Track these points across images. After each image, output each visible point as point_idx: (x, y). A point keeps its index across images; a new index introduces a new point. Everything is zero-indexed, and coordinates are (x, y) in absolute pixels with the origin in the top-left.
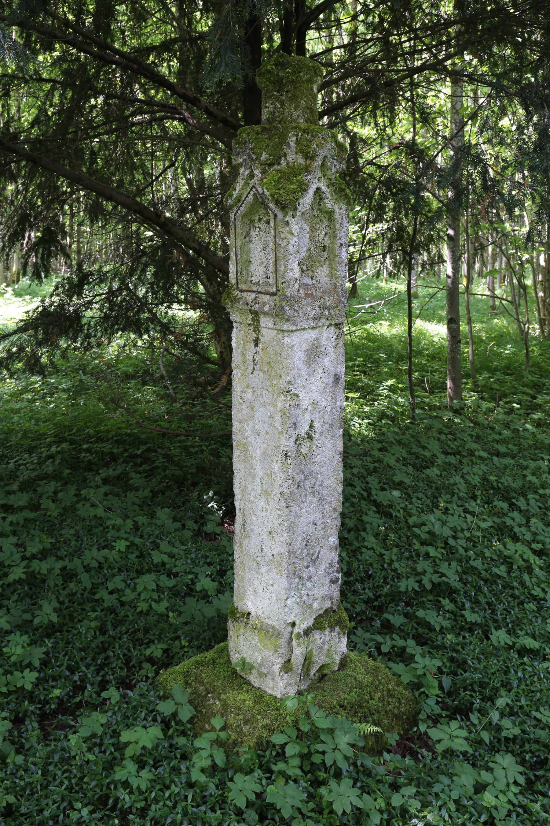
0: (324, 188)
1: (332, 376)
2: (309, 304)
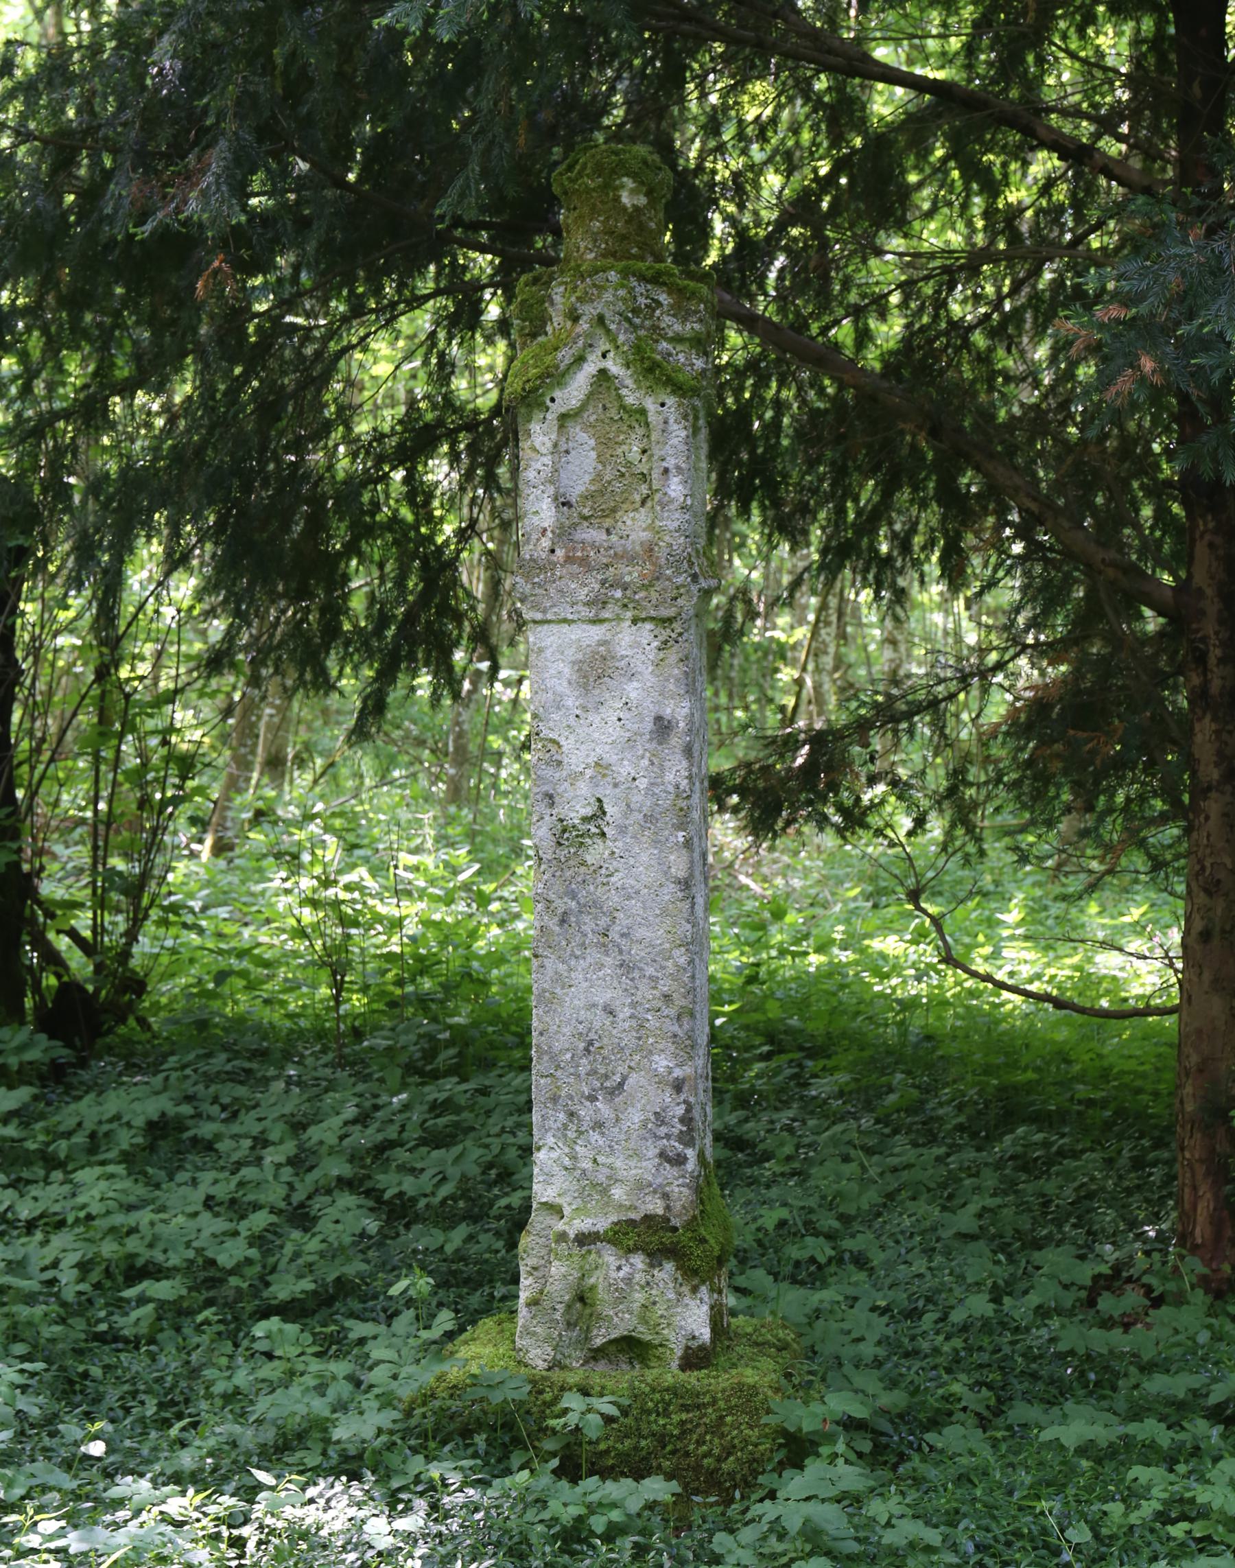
0: (614, 367)
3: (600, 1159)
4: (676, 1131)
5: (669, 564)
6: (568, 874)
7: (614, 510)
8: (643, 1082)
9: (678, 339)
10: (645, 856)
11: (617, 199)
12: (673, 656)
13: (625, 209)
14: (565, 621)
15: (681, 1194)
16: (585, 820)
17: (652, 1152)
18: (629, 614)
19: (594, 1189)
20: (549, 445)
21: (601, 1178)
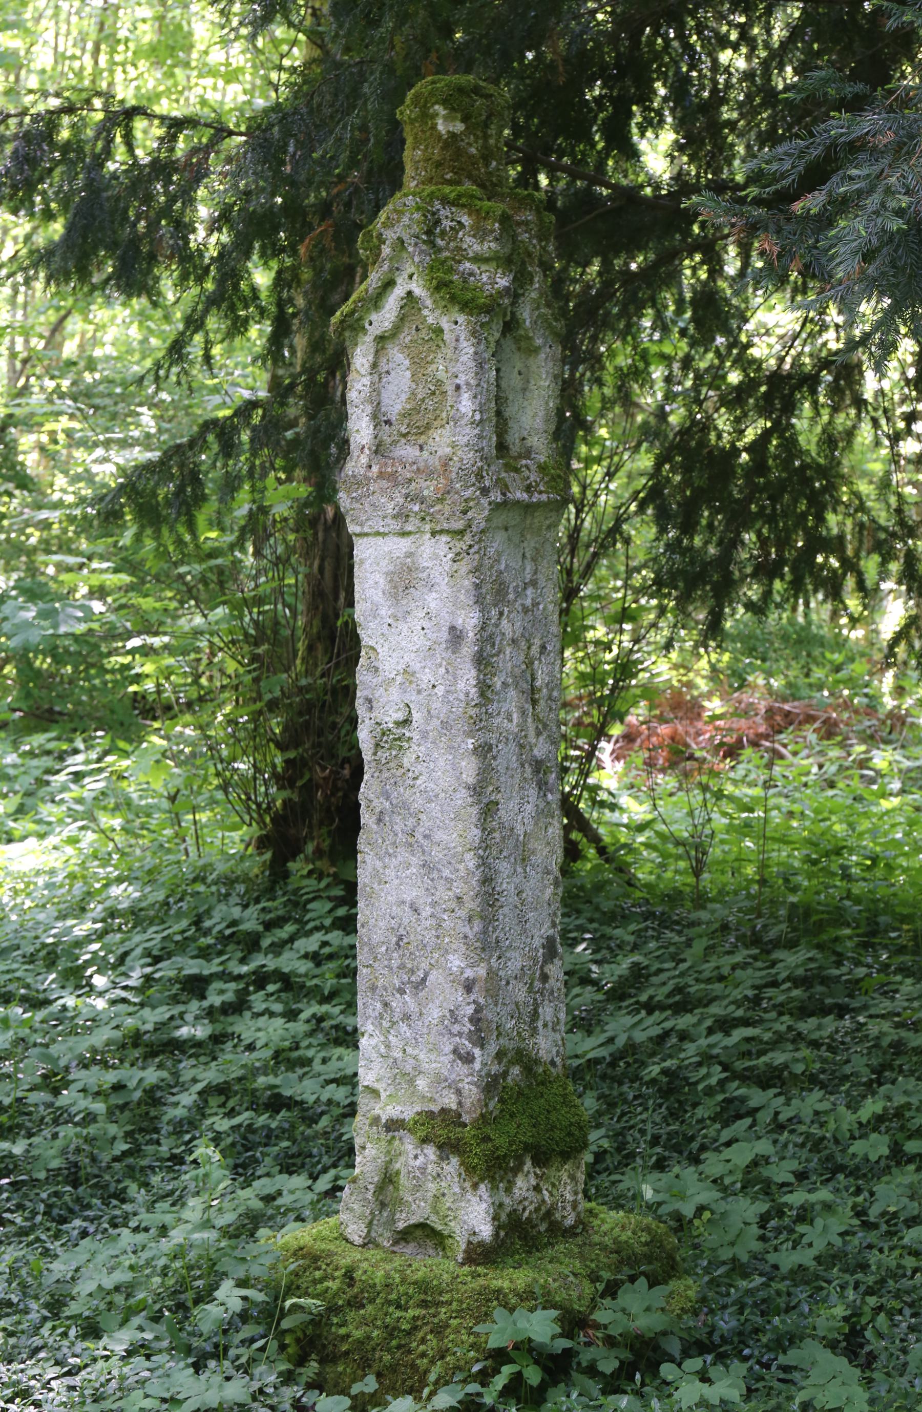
0: (418, 291)
1: (445, 629)
3: (409, 1050)
4: (466, 1030)
5: (460, 479)
6: (386, 774)
7: (428, 427)
8: (441, 979)
9: (478, 259)
10: (442, 761)
11: (434, 127)
12: (464, 567)
13: (440, 136)
14: (378, 534)
15: (472, 1092)
16: (398, 724)
17: (448, 1048)
18: (428, 527)
19: (404, 1078)
20: (367, 366)
21: (408, 1068)
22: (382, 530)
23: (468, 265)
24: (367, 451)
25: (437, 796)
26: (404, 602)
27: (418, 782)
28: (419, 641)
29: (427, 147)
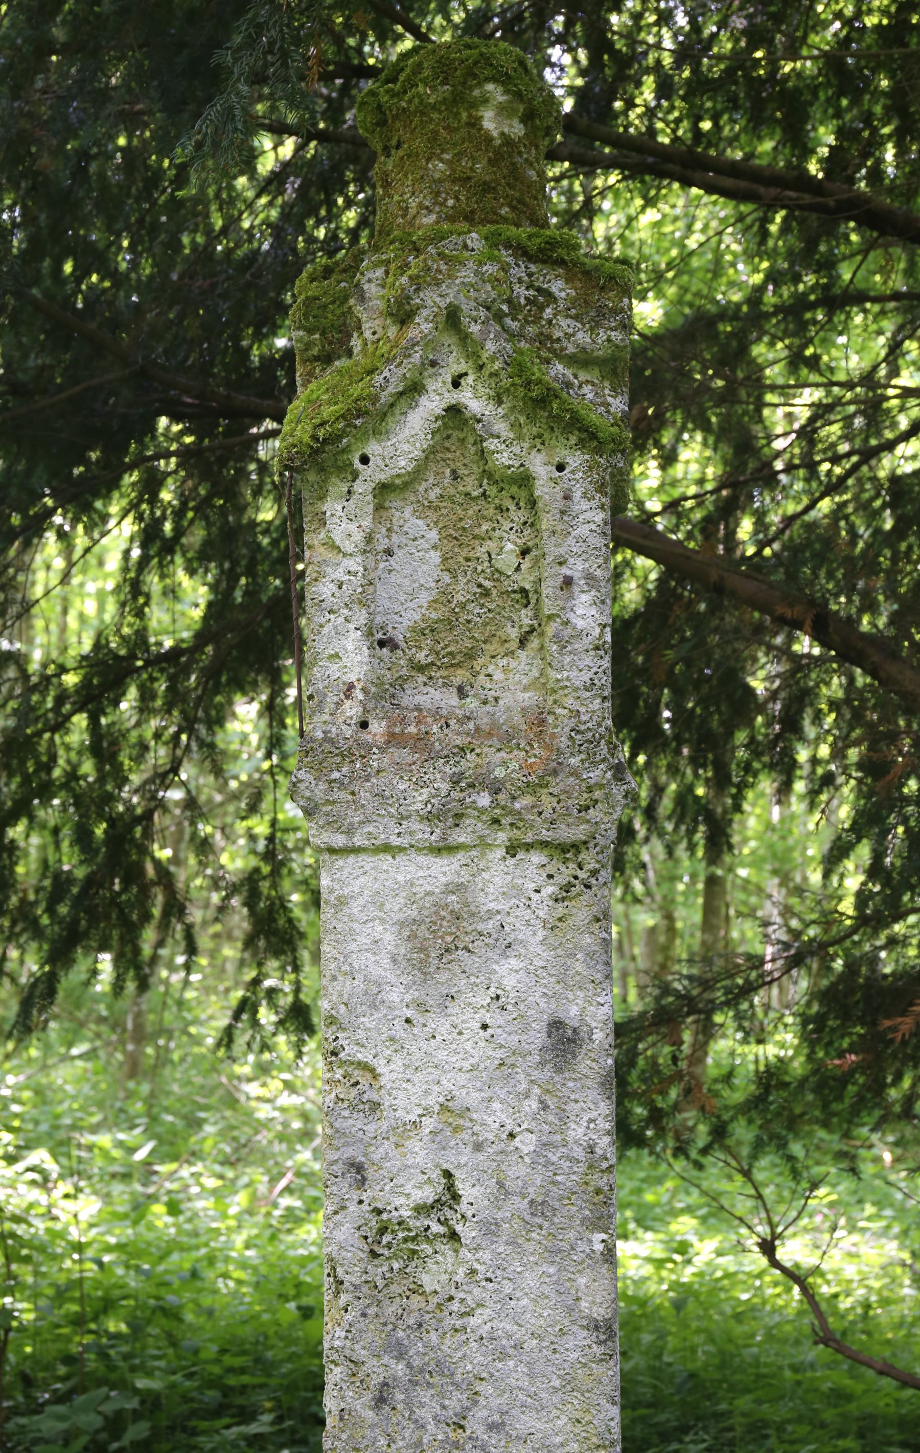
2: (400, 768)
7: (470, 655)
9: (582, 360)
11: (475, 123)
13: (489, 139)
14: (386, 848)
18: (502, 837)
22: (395, 841)
23: (559, 368)
24: (358, 694)
25: (518, 1346)
26: (443, 977)
27: (473, 1321)
28: (476, 1049)
29: (459, 156)
